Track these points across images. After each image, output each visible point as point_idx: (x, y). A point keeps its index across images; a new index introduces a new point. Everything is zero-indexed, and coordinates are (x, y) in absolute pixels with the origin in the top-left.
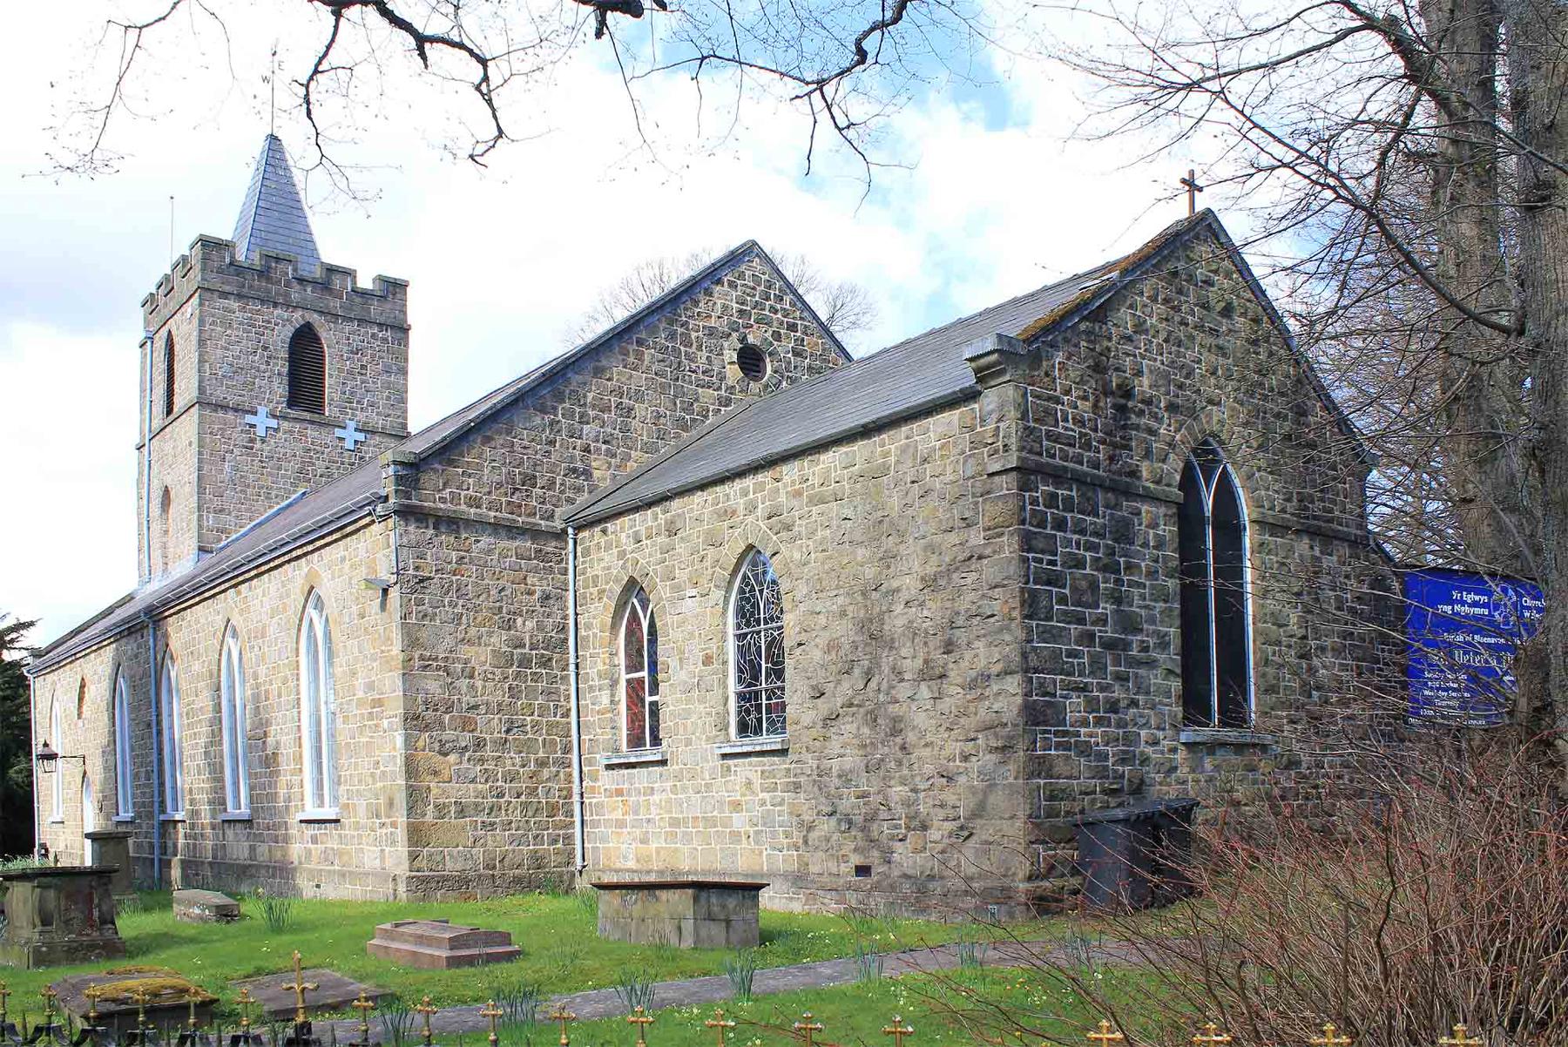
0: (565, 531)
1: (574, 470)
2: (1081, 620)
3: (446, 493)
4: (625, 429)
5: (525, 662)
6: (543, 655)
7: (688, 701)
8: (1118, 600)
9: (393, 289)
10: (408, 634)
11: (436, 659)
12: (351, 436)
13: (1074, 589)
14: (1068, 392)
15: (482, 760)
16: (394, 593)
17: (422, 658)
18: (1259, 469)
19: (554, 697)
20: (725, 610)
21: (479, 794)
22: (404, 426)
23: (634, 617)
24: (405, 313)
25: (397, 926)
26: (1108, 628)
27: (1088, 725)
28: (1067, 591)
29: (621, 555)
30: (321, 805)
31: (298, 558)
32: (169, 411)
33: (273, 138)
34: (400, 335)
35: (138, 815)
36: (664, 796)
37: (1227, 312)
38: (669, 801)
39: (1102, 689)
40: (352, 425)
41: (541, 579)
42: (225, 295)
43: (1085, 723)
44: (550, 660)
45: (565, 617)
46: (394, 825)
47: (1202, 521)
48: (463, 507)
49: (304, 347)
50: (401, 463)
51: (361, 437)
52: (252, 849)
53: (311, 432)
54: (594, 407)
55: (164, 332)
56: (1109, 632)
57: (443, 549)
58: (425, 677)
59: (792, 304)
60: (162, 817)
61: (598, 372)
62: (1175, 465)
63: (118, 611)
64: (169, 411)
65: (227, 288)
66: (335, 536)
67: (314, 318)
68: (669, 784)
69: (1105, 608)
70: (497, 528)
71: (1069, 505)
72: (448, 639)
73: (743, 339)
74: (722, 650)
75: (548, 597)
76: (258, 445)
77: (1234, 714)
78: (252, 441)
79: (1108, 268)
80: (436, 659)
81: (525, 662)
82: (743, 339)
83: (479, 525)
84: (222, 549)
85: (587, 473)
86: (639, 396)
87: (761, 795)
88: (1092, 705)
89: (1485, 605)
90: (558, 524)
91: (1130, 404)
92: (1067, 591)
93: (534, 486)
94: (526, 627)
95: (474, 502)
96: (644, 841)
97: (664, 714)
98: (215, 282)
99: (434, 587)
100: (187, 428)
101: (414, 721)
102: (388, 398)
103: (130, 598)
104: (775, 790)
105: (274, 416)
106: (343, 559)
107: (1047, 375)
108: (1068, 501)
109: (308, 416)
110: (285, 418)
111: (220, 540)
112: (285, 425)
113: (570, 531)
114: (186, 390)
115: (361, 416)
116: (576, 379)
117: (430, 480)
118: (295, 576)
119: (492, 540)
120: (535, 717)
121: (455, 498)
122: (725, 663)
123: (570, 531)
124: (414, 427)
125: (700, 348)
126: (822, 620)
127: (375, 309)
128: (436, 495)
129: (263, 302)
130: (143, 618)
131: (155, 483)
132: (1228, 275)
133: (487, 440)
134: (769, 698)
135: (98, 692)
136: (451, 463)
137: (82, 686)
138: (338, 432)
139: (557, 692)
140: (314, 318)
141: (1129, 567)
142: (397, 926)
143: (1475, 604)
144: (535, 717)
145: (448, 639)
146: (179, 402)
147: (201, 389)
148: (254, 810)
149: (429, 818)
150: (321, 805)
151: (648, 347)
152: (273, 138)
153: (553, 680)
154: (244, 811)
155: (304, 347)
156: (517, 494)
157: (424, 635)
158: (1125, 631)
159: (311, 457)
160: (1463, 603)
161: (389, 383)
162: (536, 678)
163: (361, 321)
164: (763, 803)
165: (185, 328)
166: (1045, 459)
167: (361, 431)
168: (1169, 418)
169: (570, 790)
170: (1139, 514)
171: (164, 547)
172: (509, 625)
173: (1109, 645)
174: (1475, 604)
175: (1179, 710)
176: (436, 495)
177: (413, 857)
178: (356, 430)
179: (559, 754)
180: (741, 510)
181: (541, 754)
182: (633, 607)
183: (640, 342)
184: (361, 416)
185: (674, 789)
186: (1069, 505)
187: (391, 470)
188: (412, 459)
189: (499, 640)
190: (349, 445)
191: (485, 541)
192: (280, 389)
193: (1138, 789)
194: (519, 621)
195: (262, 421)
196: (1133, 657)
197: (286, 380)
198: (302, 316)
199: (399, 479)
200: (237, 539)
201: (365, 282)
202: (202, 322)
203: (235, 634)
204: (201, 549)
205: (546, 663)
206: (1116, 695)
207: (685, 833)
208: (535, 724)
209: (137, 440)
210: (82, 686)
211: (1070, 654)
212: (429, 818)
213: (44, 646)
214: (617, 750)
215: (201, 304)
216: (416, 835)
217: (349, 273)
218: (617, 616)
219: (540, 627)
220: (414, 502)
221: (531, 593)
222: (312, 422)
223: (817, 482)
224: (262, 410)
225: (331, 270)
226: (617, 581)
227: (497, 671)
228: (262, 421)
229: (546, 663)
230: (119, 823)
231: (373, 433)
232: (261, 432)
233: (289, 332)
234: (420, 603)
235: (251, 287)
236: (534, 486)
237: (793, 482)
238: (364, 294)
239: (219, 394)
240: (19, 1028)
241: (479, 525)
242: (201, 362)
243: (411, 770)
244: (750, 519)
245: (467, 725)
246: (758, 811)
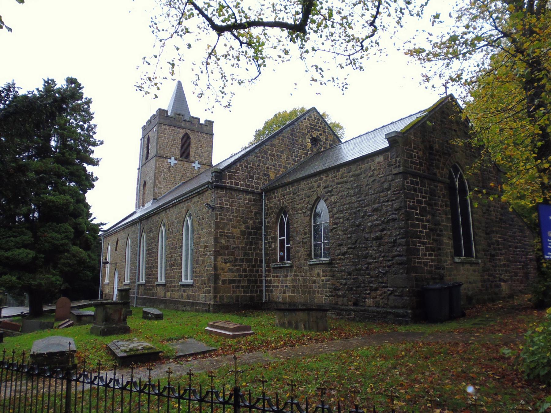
0: (262, 193)
1: (265, 174)
7: (299, 247)
8: (433, 215)
9: (210, 124)
15: (236, 266)
21: (235, 276)
23: (282, 220)
25: (214, 323)
27: (426, 256)
28: (418, 211)
29: (279, 200)
30: (187, 279)
31: (185, 201)
34: (211, 136)
35: (131, 282)
36: (291, 278)
38: (293, 280)
39: (430, 244)
43: (425, 255)
45: (262, 219)
46: (210, 287)
47: (456, 189)
49: (186, 141)
51: (199, 166)
52: (165, 294)
55: (147, 136)
59: (325, 125)
60: (138, 283)
62: (445, 171)
67: (188, 131)
68: (292, 274)
71: (417, 183)
73: (311, 135)
76: (171, 168)
77: (469, 253)
78: (170, 167)
79: (425, 111)
82: (311, 135)
83: (239, 190)
85: (268, 176)
87: (323, 278)
92: (418, 211)
95: (237, 184)
96: (285, 293)
97: (292, 250)
98: (162, 121)
100: (152, 164)
101: (217, 253)
104: (326, 276)
106: (198, 202)
108: (417, 182)
110: (179, 160)
112: (180, 162)
114: (152, 153)
118: (185, 205)
124: (214, 163)
125: (299, 138)
126: (341, 220)
127: (205, 129)
129: (175, 127)
131: (142, 179)
134: (324, 246)
137: (118, 241)
139: (258, 243)
140: (188, 131)
141: (435, 204)
142: (214, 323)
146: (150, 156)
147: (157, 152)
148: (167, 281)
149: (220, 284)
150: (187, 279)
154: (163, 281)
155: (186, 141)
163: (201, 132)
164: (323, 281)
165: (153, 134)
166: (410, 169)
169: (262, 275)
173: (431, 230)
175: (453, 251)
177: (215, 297)
179: (253, 263)
180: (316, 187)
181: (253, 263)
182: (282, 216)
185: (294, 276)
186: (417, 183)
190: (196, 168)
192: (178, 152)
193: (441, 278)
202: (158, 133)
203: (190, 216)
207: (297, 290)
208: (252, 253)
209: (138, 167)
210: (118, 241)
211: (420, 232)
212: (220, 284)
216: (216, 290)
217: (199, 119)
218: (277, 219)
219: (254, 222)
223: (339, 177)
224: (173, 158)
225: (194, 118)
226: (277, 208)
228: (173, 161)
230: (125, 285)
232: (172, 164)
233: (181, 136)
237: (332, 178)
238: (202, 124)
239: (162, 153)
240: (120, 381)
242: (157, 144)
243: (215, 268)
244: (319, 189)
245: (232, 254)
246: (321, 283)
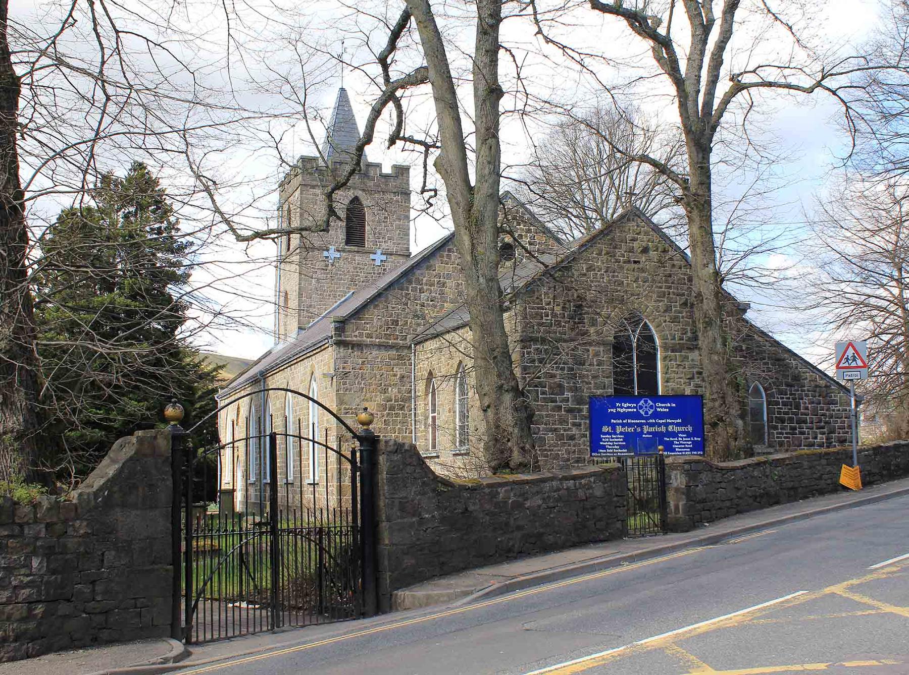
0: (411, 345)
2: (554, 401)
3: (357, 333)
4: (442, 293)
5: (392, 408)
6: (400, 405)
10: (340, 399)
11: (351, 409)
12: (379, 257)
13: (550, 388)
14: (549, 304)
16: (335, 378)
17: (345, 409)
18: (665, 321)
19: (405, 424)
20: (455, 388)
22: (408, 249)
24: (408, 185)
26: (569, 403)
32: (289, 249)
33: (343, 90)
34: (406, 197)
37: (645, 250)
40: (379, 252)
41: (400, 368)
42: (313, 187)
44: (404, 406)
48: (365, 338)
50: (337, 322)
51: (384, 258)
53: (358, 258)
54: (426, 284)
56: (570, 405)
57: (355, 358)
58: (347, 417)
61: (429, 268)
63: (263, 361)
64: (289, 249)
65: (314, 183)
66: (317, 351)
69: (568, 394)
70: (380, 346)
72: (357, 400)
74: (454, 407)
75: (403, 377)
78: (327, 266)
80: (351, 409)
81: (392, 408)
83: (372, 346)
84: (310, 327)
86: (449, 276)
88: (561, 438)
89: (634, 407)
90: (408, 342)
91: (584, 304)
93: (397, 325)
94: (393, 392)
95: (369, 336)
99: (351, 375)
102: (399, 234)
103: (269, 353)
105: (338, 251)
107: (537, 298)
109: (356, 248)
110: (344, 251)
111: (309, 323)
113: (413, 346)
115: (384, 245)
116: (418, 272)
117: (350, 327)
119: (378, 352)
120: (396, 434)
121: (361, 335)
122: (455, 412)
123: (413, 346)
128: (352, 335)
130: (259, 376)
132: (646, 233)
133: (376, 306)
135: (244, 413)
136: (360, 319)
138: (372, 256)
139: (406, 422)
140: (359, 193)
143: (628, 407)
144: (396, 434)
145: (357, 400)
151: (454, 252)
152: (343, 90)
153: (405, 416)
156: (390, 330)
157: (346, 398)
158: (578, 404)
159: (357, 272)
160: (622, 407)
161: (400, 225)
162: (397, 415)
167: (384, 254)
168: (607, 307)
170: (589, 351)
171: (285, 325)
172: (385, 391)
173: (570, 411)
174: (628, 407)
176: (352, 335)
178: (382, 254)
183: (449, 250)
184: (384, 245)
187: (333, 324)
188: (342, 319)
189: (380, 399)
190: (378, 263)
191: (375, 352)
194: (390, 389)
195: (333, 254)
196: (583, 415)
197: (344, 230)
198: (353, 193)
199: (336, 329)
200: (318, 321)
201: (387, 170)
204: (300, 328)
205: (402, 408)
206: (574, 433)
210: (238, 408)
213: (256, 359)
214: (428, 450)
215: (301, 193)
217: (379, 166)
220: (343, 338)
221: (395, 375)
222: (358, 252)
224: (332, 248)
227: (379, 413)
228: (333, 254)
229: (402, 408)
231: (391, 254)
234: (345, 384)
235: (326, 180)
236: (397, 325)
238: (387, 176)
241: (372, 346)
